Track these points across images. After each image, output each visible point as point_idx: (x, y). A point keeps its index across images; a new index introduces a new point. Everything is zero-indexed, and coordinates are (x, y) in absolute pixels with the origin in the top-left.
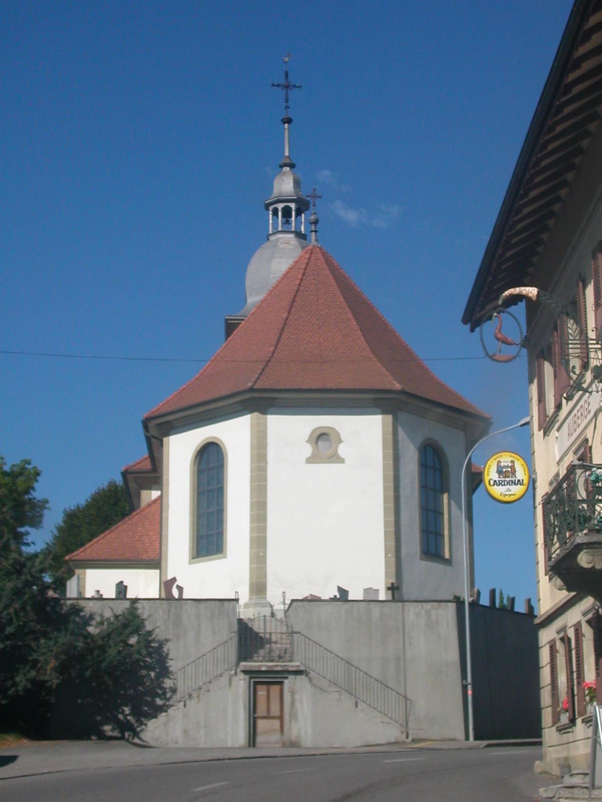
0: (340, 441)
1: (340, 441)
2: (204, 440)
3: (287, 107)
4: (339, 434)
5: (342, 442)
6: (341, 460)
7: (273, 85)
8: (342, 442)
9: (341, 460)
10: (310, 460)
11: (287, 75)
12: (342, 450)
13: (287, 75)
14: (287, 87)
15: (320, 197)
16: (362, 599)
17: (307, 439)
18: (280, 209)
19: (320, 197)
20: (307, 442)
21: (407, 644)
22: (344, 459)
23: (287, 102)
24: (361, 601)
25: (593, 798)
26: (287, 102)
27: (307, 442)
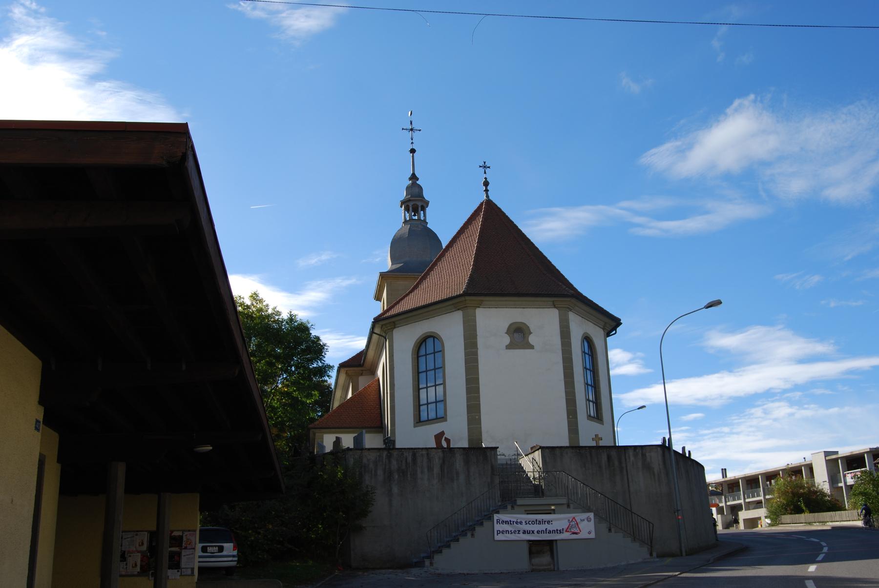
0: (530, 333)
1: (530, 333)
2: (423, 335)
3: (412, 143)
4: (529, 327)
5: (532, 333)
6: (531, 347)
7: (403, 129)
8: (532, 333)
9: (531, 347)
10: (509, 347)
11: (411, 123)
12: (532, 339)
13: (411, 123)
14: (412, 130)
15: (489, 167)
16: (568, 445)
17: (505, 331)
18: (420, 206)
19: (489, 167)
20: (506, 333)
21: (630, 480)
22: (533, 346)
23: (412, 140)
24: (567, 447)
25: (184, 575)
26: (412, 140)
27: (506, 333)
